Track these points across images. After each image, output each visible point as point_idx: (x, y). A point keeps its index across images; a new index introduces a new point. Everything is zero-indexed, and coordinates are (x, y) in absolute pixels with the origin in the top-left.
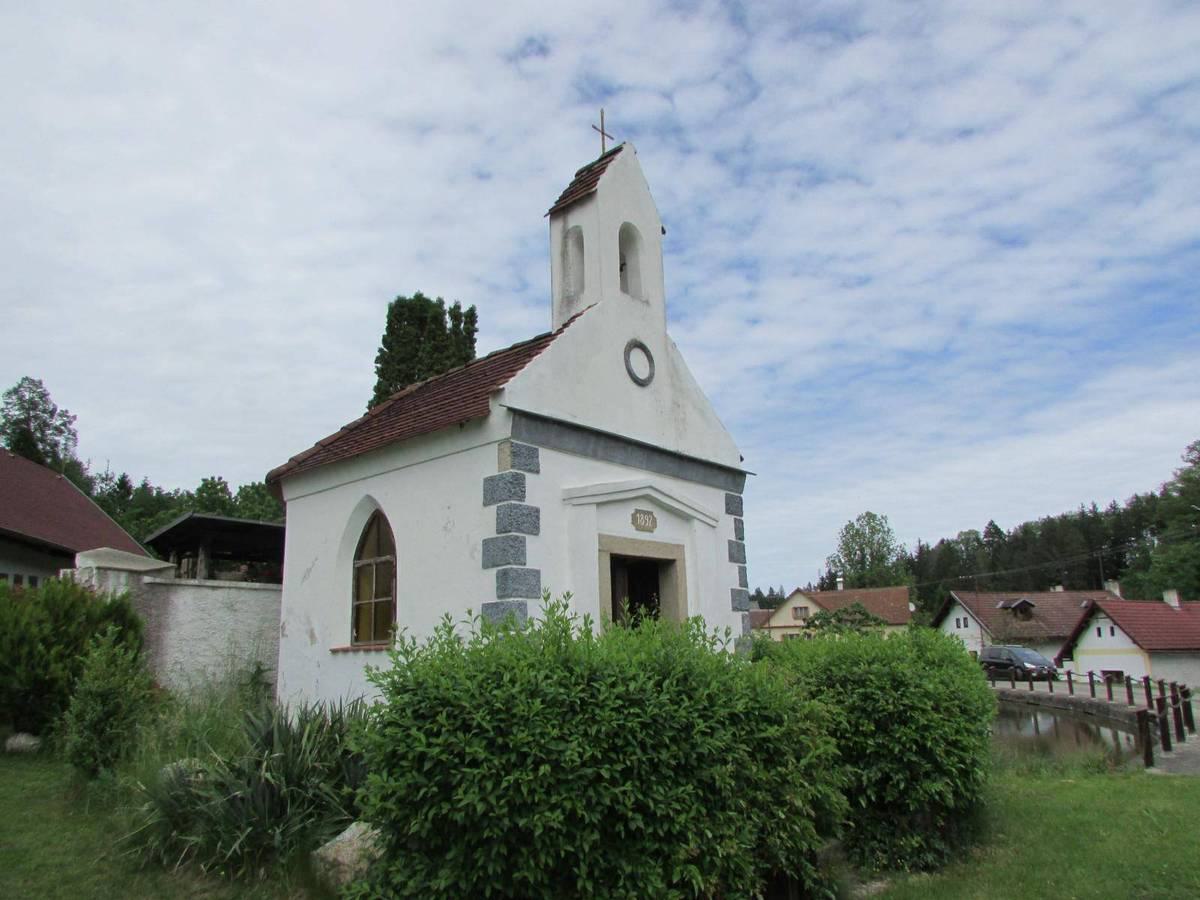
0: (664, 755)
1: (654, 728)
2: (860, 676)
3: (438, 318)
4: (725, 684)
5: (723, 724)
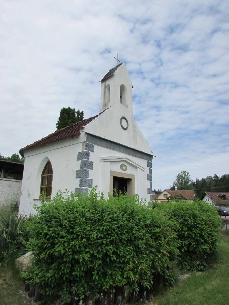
0: (124, 237)
1: (121, 228)
2: (184, 214)
3: (73, 114)
4: (144, 215)
5: (143, 227)
